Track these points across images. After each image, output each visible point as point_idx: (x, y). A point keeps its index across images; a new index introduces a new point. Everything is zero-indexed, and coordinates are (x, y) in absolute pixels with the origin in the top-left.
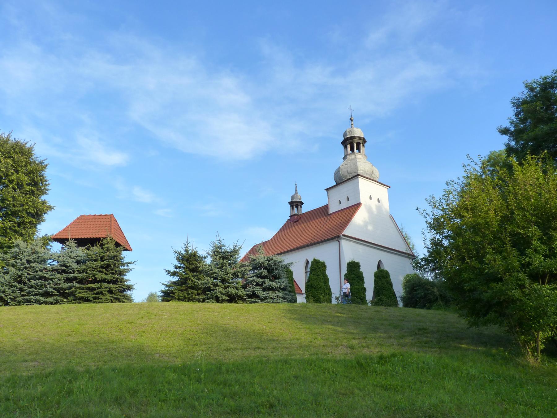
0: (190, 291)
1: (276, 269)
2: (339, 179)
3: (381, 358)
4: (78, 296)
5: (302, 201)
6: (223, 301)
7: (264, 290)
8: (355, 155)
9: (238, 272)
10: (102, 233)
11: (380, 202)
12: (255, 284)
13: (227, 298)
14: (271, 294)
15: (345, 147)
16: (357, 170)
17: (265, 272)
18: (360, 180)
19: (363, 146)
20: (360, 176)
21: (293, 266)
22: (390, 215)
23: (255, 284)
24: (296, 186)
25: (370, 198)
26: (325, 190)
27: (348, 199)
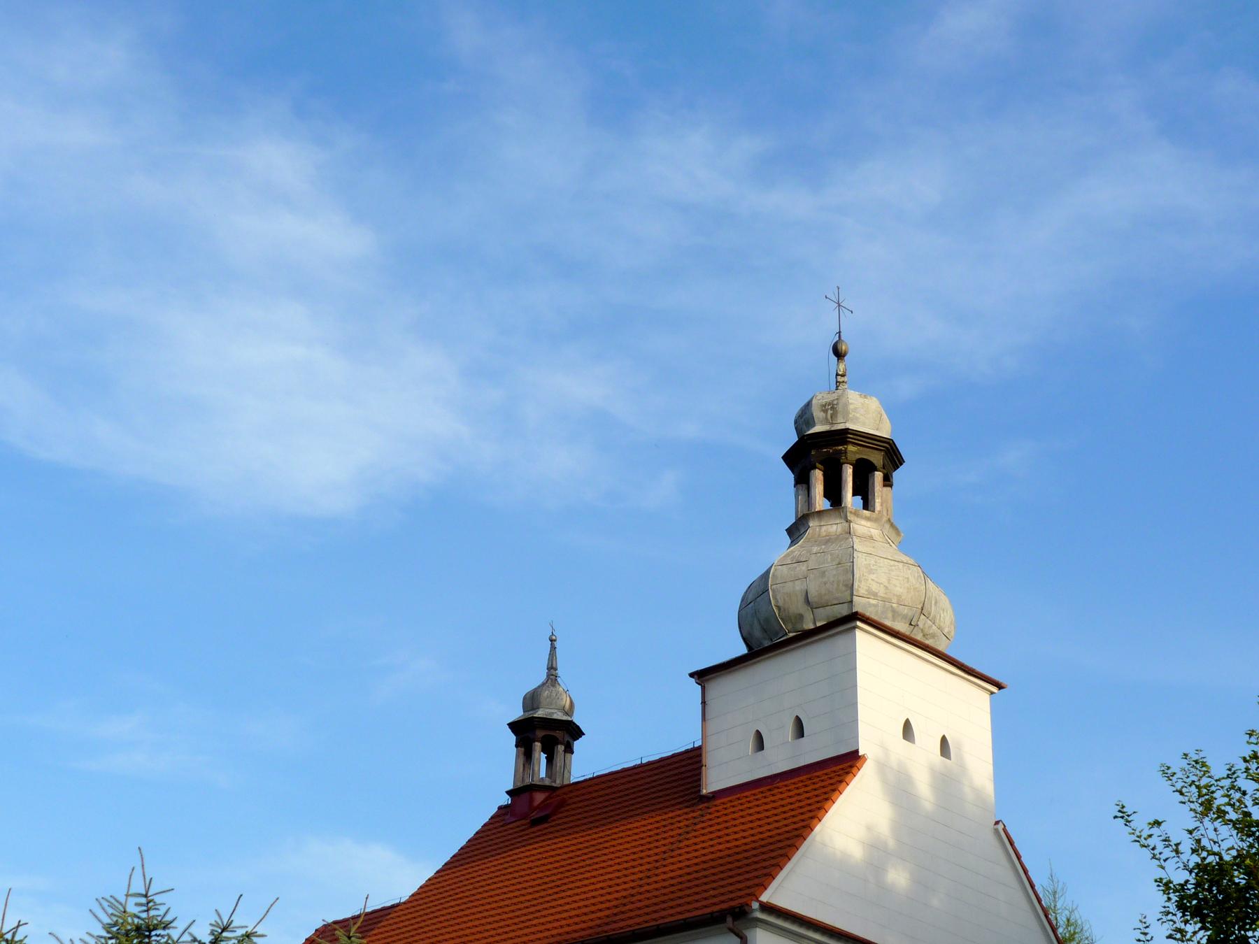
2: (765, 631)
5: (577, 719)
15: (802, 480)
16: (852, 595)
18: (865, 642)
19: (887, 481)
22: (997, 823)
24: (553, 648)
26: (692, 675)
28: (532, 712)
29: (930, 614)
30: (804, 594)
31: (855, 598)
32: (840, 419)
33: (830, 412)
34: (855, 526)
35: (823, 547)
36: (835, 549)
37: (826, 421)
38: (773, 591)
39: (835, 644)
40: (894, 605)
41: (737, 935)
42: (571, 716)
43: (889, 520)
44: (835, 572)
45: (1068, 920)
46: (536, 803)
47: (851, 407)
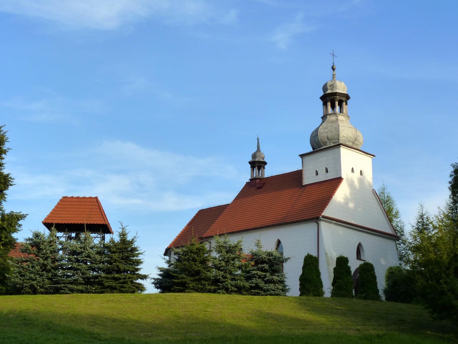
0: (203, 282)
1: (276, 264)
2: (317, 144)
3: (378, 336)
4: (106, 285)
5: (265, 160)
6: (232, 291)
7: (267, 282)
8: (337, 116)
9: (242, 265)
10: (95, 219)
12: (257, 277)
13: (236, 289)
14: (272, 286)
15: (325, 104)
16: (339, 137)
17: (266, 266)
18: (343, 150)
19: (346, 104)
21: (290, 261)
23: (257, 277)
24: (258, 141)
25: (353, 170)
26: (299, 156)
27: (327, 171)
28: (254, 159)
29: (357, 140)
31: (340, 138)
33: (332, 87)
34: (339, 118)
35: (331, 124)
36: (334, 125)
37: (331, 89)
38: (319, 135)
39: (336, 150)
40: (349, 139)
41: (317, 223)
42: (263, 159)
43: (347, 115)
44: (334, 131)
45: (388, 196)
47: (337, 86)
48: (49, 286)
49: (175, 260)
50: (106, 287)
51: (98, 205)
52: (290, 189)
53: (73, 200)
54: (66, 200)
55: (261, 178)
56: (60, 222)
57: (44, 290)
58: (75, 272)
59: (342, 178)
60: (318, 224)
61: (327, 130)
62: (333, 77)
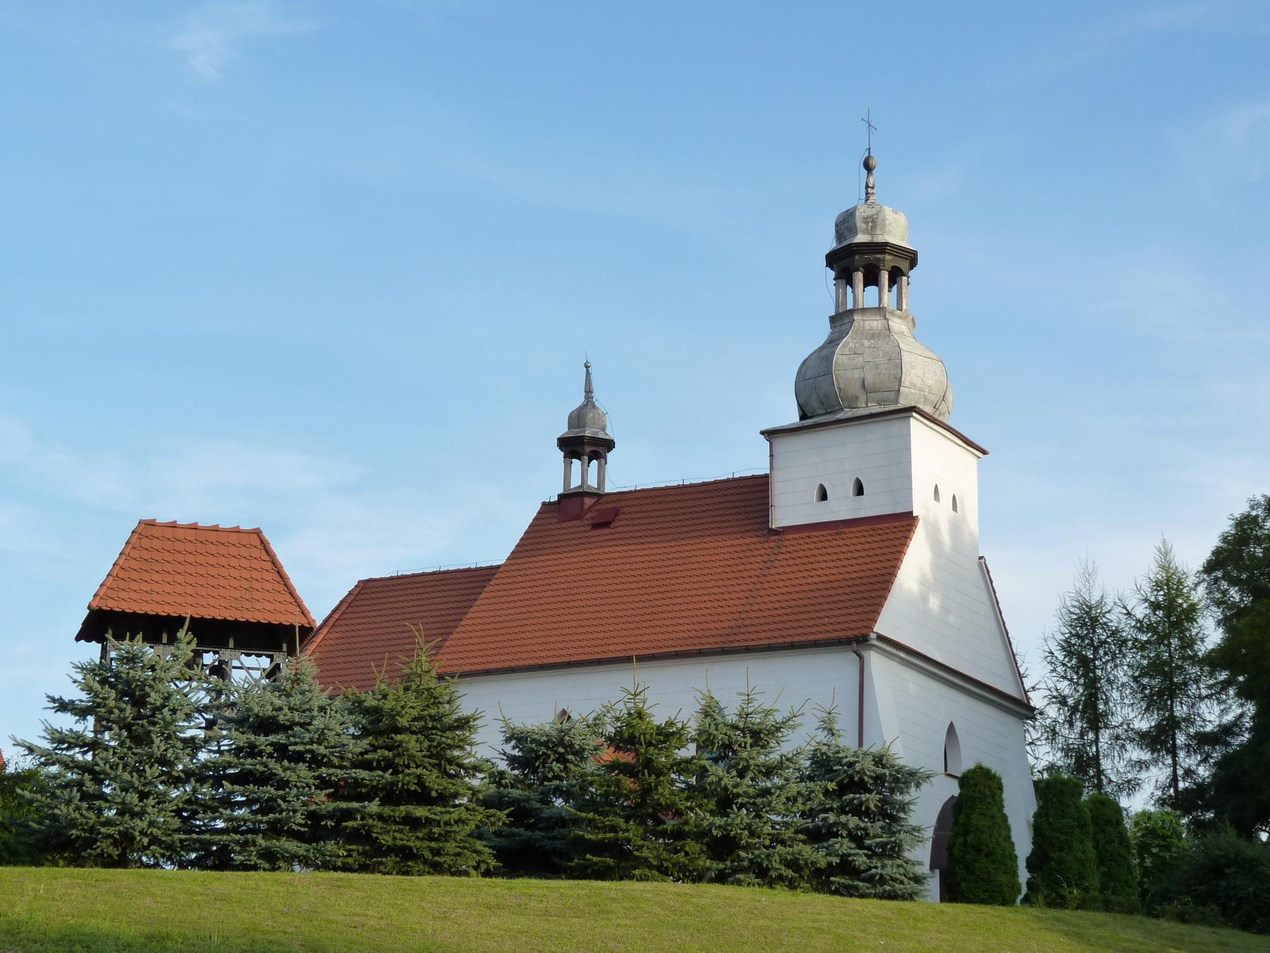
5: (611, 433)
8: (885, 319)
11: (939, 501)
16: (900, 385)
18: (917, 427)
20: (916, 412)
24: (588, 374)
26: (762, 433)
30: (861, 382)
32: (878, 231)
33: (870, 224)
37: (866, 232)
39: (894, 426)
46: (586, 507)
47: (888, 222)
48: (183, 837)
49: (505, 758)
50: (384, 849)
51: (267, 558)
52: (726, 537)
53: (180, 534)
54: (152, 530)
55: (599, 492)
56: (208, 613)
57: (162, 851)
58: (281, 792)
59: (914, 515)
60: (861, 658)
61: (861, 360)
62: (867, 194)
